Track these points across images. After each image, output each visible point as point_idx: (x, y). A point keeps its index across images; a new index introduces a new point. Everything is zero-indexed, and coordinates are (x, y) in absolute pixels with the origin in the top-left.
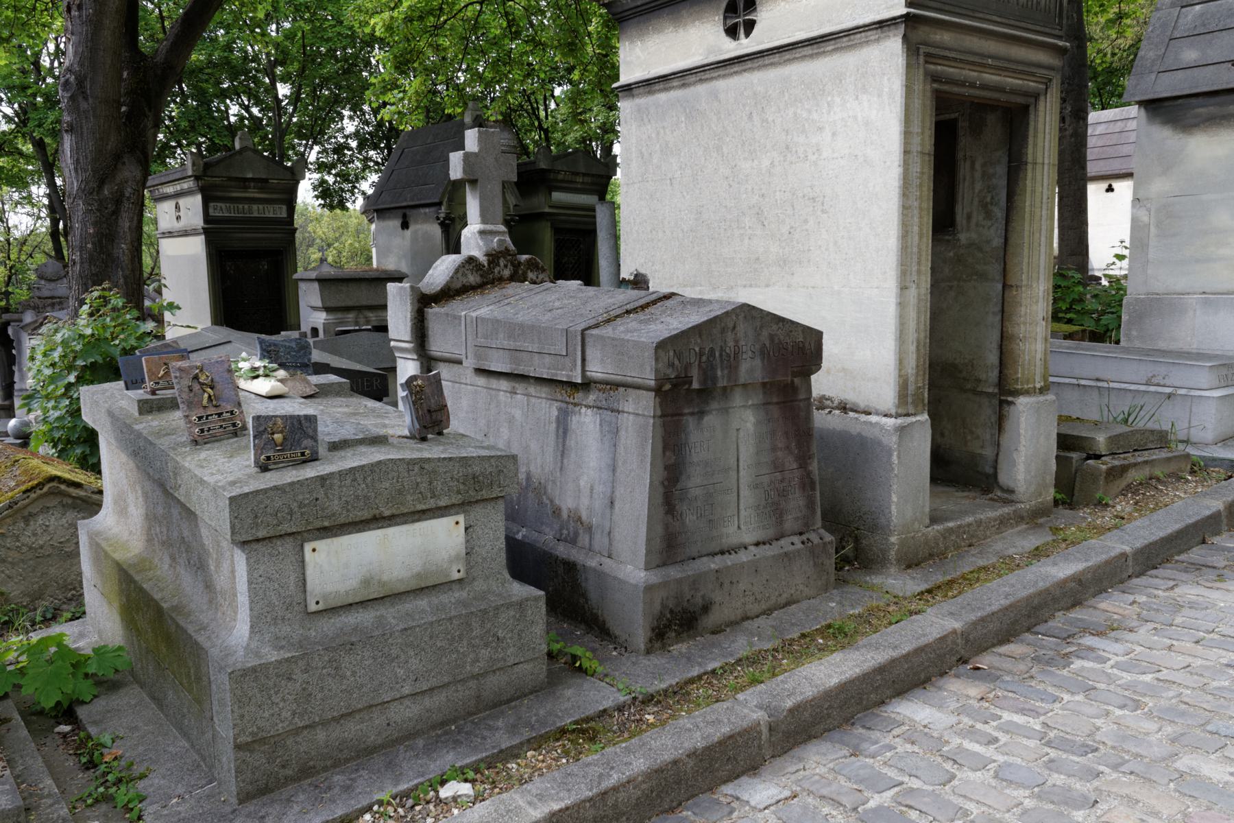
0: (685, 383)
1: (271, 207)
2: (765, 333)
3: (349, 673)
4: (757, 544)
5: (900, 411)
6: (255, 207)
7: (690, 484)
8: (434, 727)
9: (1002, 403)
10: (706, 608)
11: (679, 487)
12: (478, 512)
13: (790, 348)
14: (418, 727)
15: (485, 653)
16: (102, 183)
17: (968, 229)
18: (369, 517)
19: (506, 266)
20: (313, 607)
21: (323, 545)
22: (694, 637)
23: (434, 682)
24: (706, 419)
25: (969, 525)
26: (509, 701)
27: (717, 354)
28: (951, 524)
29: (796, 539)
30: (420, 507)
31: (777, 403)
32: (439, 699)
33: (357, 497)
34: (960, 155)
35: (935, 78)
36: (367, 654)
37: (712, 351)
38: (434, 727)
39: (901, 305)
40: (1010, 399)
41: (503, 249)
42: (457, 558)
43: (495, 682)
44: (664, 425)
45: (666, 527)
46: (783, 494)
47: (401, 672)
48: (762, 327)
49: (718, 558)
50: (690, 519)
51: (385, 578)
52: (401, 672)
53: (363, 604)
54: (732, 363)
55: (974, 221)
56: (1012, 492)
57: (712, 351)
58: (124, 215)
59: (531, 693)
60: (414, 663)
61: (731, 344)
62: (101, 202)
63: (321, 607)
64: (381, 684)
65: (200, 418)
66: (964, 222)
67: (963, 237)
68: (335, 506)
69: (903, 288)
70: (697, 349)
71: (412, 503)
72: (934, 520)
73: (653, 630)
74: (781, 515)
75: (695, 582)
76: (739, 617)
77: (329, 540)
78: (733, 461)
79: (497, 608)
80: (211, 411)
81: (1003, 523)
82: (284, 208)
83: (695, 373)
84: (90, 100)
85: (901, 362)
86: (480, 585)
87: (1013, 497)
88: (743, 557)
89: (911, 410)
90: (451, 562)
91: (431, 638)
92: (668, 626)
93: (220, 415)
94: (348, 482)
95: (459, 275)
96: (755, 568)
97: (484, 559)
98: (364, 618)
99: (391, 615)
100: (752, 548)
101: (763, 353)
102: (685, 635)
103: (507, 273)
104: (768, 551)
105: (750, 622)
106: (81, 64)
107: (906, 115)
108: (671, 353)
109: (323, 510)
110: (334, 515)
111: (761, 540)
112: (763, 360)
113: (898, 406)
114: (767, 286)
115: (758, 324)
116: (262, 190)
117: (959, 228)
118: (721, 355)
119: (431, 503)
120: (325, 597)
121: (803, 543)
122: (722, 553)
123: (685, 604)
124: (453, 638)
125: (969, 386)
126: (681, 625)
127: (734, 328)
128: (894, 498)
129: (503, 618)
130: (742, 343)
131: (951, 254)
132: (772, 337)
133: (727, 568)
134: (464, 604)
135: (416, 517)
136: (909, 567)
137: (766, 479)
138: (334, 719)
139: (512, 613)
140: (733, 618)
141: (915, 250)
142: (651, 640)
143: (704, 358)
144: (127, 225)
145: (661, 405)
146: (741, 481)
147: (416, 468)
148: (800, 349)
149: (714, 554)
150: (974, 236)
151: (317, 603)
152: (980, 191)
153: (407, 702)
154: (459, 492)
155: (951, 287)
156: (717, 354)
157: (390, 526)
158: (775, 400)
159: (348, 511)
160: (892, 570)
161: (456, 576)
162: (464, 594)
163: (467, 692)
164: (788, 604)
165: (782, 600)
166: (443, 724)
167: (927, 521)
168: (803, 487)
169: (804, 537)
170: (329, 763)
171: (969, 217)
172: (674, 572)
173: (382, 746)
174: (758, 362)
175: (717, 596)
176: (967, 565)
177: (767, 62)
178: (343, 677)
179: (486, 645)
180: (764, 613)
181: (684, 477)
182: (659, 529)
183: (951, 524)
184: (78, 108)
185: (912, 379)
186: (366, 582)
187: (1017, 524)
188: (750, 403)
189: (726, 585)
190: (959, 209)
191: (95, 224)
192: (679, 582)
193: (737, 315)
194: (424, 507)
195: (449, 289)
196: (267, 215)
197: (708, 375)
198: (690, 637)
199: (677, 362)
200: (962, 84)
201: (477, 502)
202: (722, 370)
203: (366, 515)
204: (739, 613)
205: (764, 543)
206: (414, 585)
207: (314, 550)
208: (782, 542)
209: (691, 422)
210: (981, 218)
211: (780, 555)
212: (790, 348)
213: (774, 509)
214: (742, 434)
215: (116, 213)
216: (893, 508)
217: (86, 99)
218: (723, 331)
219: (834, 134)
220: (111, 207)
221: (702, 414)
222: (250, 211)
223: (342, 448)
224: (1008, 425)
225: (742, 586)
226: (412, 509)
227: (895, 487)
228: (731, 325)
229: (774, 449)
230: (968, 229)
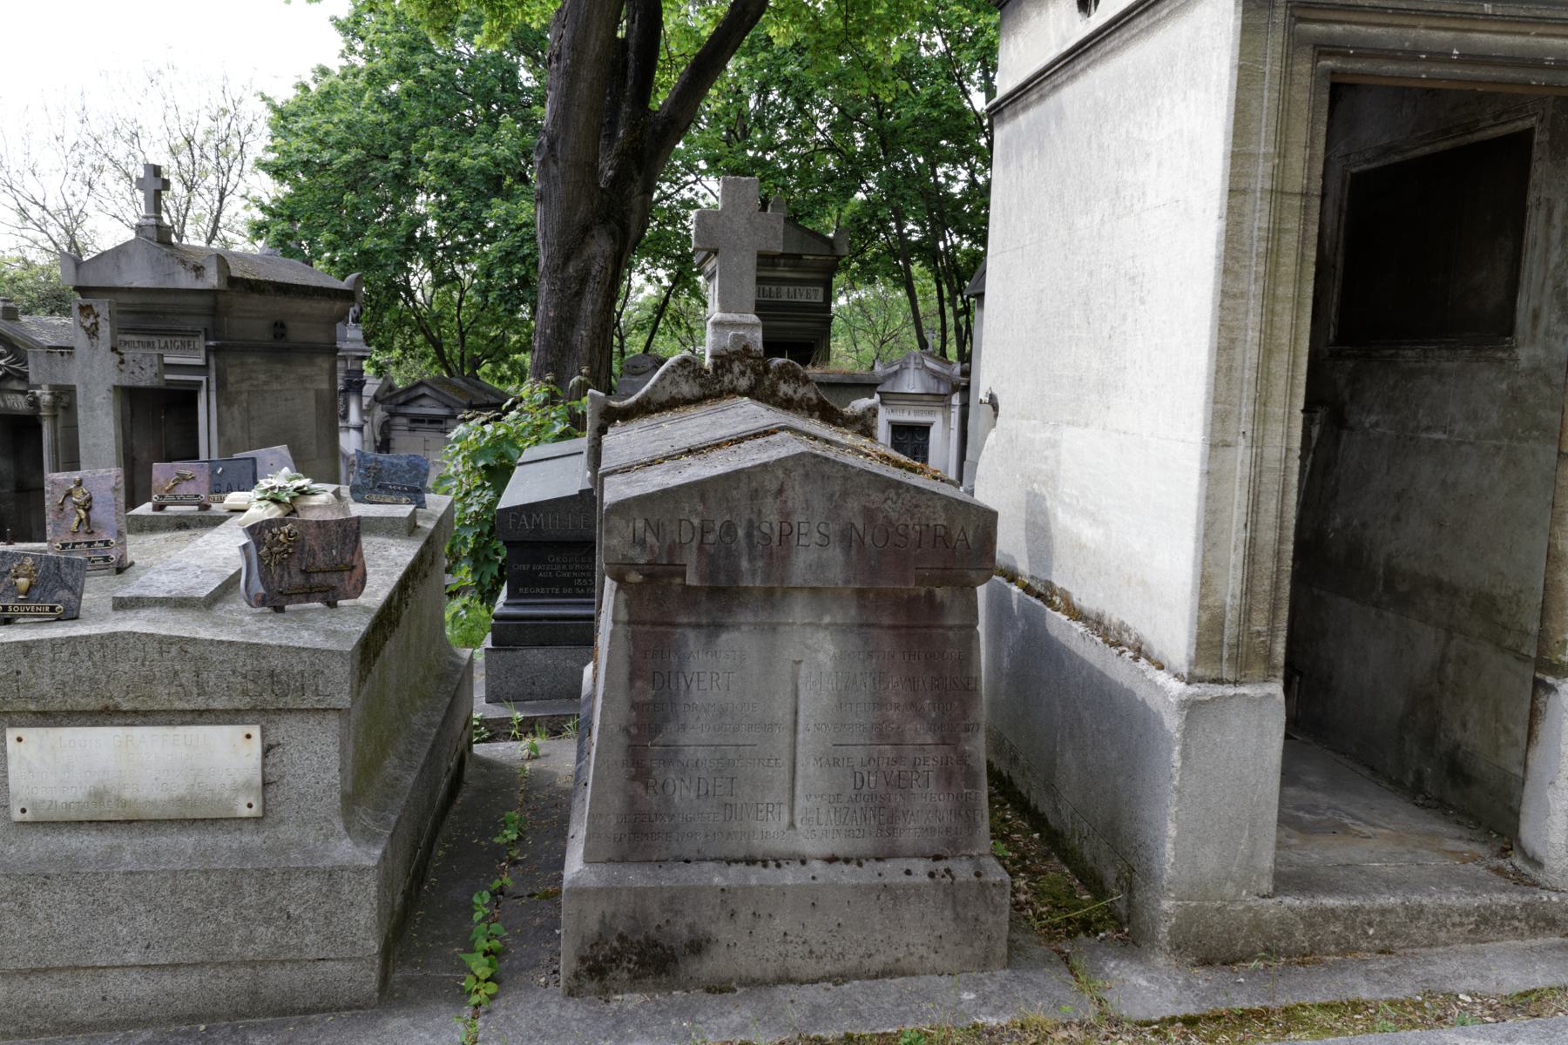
0: (672, 575)
1: (804, 289)
2: (853, 505)
3: (40, 916)
4: (831, 860)
5: (1199, 672)
6: (784, 289)
7: (683, 739)
8: (177, 1019)
9: (1539, 685)
10: (698, 947)
11: (659, 739)
12: (285, 729)
13: (913, 535)
14: (153, 1013)
15: (265, 933)
16: (567, 259)
17: (1533, 342)
18: (98, 707)
19: (743, 373)
20: (17, 816)
21: (30, 734)
22: (670, 988)
23: (178, 956)
24: (725, 637)
25: (1384, 912)
26: (307, 1011)
27: (741, 533)
28: (1330, 902)
29: (921, 867)
30: (178, 705)
31: (894, 627)
32: (187, 982)
33: (79, 678)
34: (1532, 197)
35: (1324, 49)
36: (69, 896)
37: (729, 528)
38: (177, 1019)
39: (1213, 477)
40: (1550, 680)
41: (739, 348)
42: (247, 786)
43: (279, 980)
44: (633, 638)
45: (632, 801)
46: (900, 783)
47: (124, 931)
48: (845, 494)
49: (734, 870)
50: (682, 794)
51: (127, 794)
52: (124, 931)
53: (99, 824)
54: (777, 548)
55: (1543, 324)
56: (1538, 864)
57: (729, 528)
58: (588, 296)
59: (349, 1008)
60: (145, 923)
61: (774, 518)
62: (564, 281)
63: (28, 817)
64: (91, 941)
65: (64, 546)
66: (1528, 326)
67: (1523, 354)
68: (45, 685)
69: (1217, 445)
70: (696, 522)
71: (163, 696)
72: (1285, 881)
73: (583, 960)
74: (892, 818)
75: (674, 901)
76: (771, 975)
77: (42, 730)
78: (782, 713)
79: (287, 872)
80: (82, 538)
81: (1486, 924)
82: (821, 290)
83: (690, 559)
84: (560, 164)
85: (1206, 583)
86: (288, 832)
87: (1539, 876)
88: (790, 876)
89: (1228, 673)
90: (236, 790)
91: (173, 893)
92: (615, 959)
93: (90, 544)
94: (65, 655)
95: (667, 383)
96: (812, 900)
97: (302, 796)
98: (91, 844)
99: (130, 847)
100: (817, 866)
101: (847, 538)
102: (650, 980)
103: (744, 383)
104: (847, 875)
105: (791, 988)
106: (554, 124)
107: (1237, 121)
108: (640, 524)
109: (27, 687)
110: (43, 697)
111: (840, 853)
112: (847, 550)
113: (1195, 662)
114: (1086, 425)
115: (837, 487)
116: (794, 268)
117: (1520, 337)
118: (749, 535)
119: (200, 703)
120: (35, 805)
121: (931, 875)
122: (750, 861)
123: (652, 932)
124: (211, 902)
125: (1509, 642)
126: (641, 964)
127: (780, 491)
128: (1172, 830)
129: (298, 887)
130: (795, 519)
131: (1504, 386)
132: (869, 514)
133: (748, 889)
134: (245, 853)
135: (189, 718)
136: (1206, 962)
137: (858, 754)
138: (19, 971)
139: (315, 883)
140: (757, 973)
141: (1249, 375)
142: (577, 976)
143: (711, 538)
144: (590, 308)
145: (628, 605)
146: (800, 749)
147: (174, 650)
148: (942, 539)
149: (730, 861)
150: (1540, 352)
151: (23, 811)
152: (1558, 267)
153: (134, 974)
154: (245, 693)
155: (1499, 448)
156: (741, 533)
157: (145, 724)
158: (886, 621)
159: (64, 694)
160: (1160, 961)
161: (245, 812)
162: (258, 840)
163: (234, 983)
164: (886, 973)
165: (877, 963)
166: (194, 1018)
167: (1267, 885)
168: (947, 777)
169: (941, 866)
170: (12, 1029)
171: (1536, 316)
172: (636, 876)
173: (93, 1026)
174: (835, 554)
175: (723, 931)
176: (1320, 989)
177: (1108, 48)
178: (32, 919)
179: (268, 921)
180: (827, 978)
181: (672, 726)
182: (616, 802)
183: (1330, 902)
184: (547, 174)
185: (1231, 616)
186: (98, 796)
187: (1534, 931)
188: (827, 619)
189: (744, 914)
190: (1521, 302)
191: (556, 306)
192: (641, 894)
193: (787, 472)
194: (187, 707)
195: (649, 402)
196: (799, 299)
197: (719, 562)
198: (658, 987)
199: (651, 539)
200: (1411, 56)
201: (290, 711)
202: (751, 560)
203: (93, 704)
204: (772, 969)
205: (847, 861)
206: (172, 813)
207: (20, 740)
208: (888, 865)
209: (693, 641)
210: (1554, 318)
211: (871, 888)
212: (913, 535)
213: (876, 805)
214: (804, 670)
215: (579, 294)
216: (1169, 851)
217: (555, 162)
218: (754, 495)
219: (1160, 164)
220: (574, 287)
221: (716, 628)
222: (778, 294)
223: (132, 607)
224: (1544, 731)
225: (780, 924)
226: (167, 706)
227: (1173, 810)
228: (775, 486)
229: (879, 704)
230: (1533, 342)
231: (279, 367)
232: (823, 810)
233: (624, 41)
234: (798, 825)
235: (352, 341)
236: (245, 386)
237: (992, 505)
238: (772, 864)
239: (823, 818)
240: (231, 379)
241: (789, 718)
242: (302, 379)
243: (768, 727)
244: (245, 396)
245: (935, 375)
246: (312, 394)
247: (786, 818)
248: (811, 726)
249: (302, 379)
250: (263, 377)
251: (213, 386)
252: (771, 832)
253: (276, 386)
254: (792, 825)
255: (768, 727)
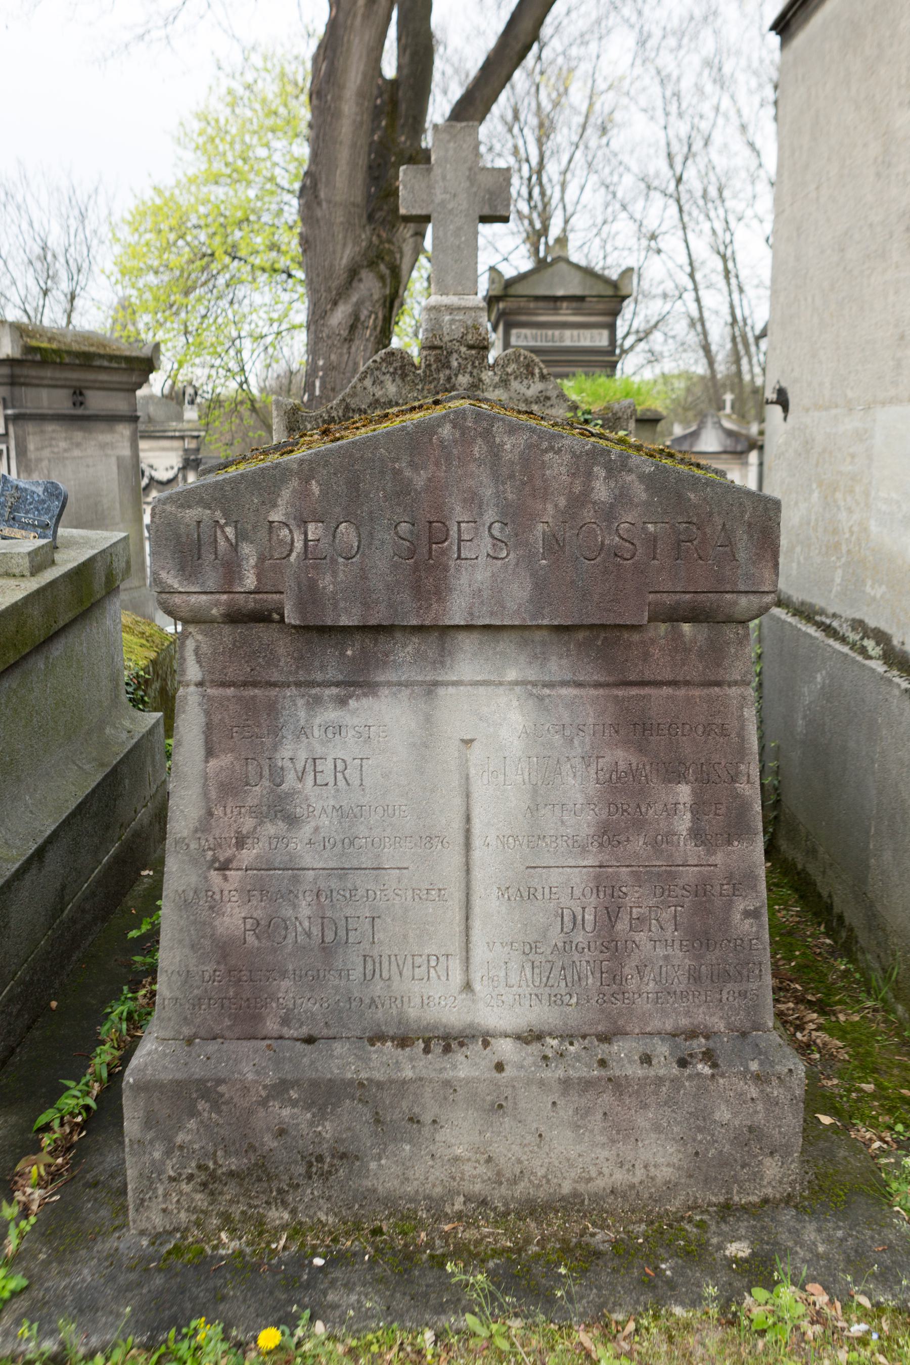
146: (478, 874)
222: (562, 339)
231: (78, 436)
232: (514, 965)
233: (394, 83)
234: (477, 987)
235: (189, 421)
236: (46, 453)
237: (779, 497)
238: (437, 1048)
239: (514, 979)
240: (31, 447)
241: (457, 825)
242: (103, 446)
243: (430, 840)
244: (45, 463)
245: (729, 433)
246: (113, 460)
247: (457, 977)
248: (492, 840)
249: (103, 446)
250: (63, 445)
251: (13, 454)
252: (437, 999)
253: (76, 453)
254: (468, 986)
255: (430, 840)
